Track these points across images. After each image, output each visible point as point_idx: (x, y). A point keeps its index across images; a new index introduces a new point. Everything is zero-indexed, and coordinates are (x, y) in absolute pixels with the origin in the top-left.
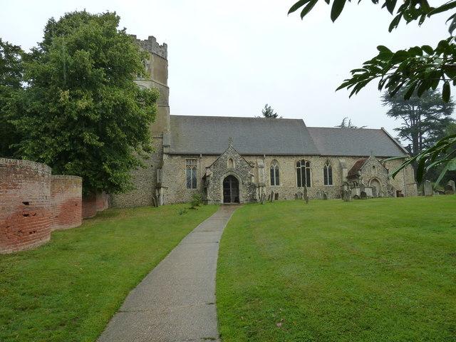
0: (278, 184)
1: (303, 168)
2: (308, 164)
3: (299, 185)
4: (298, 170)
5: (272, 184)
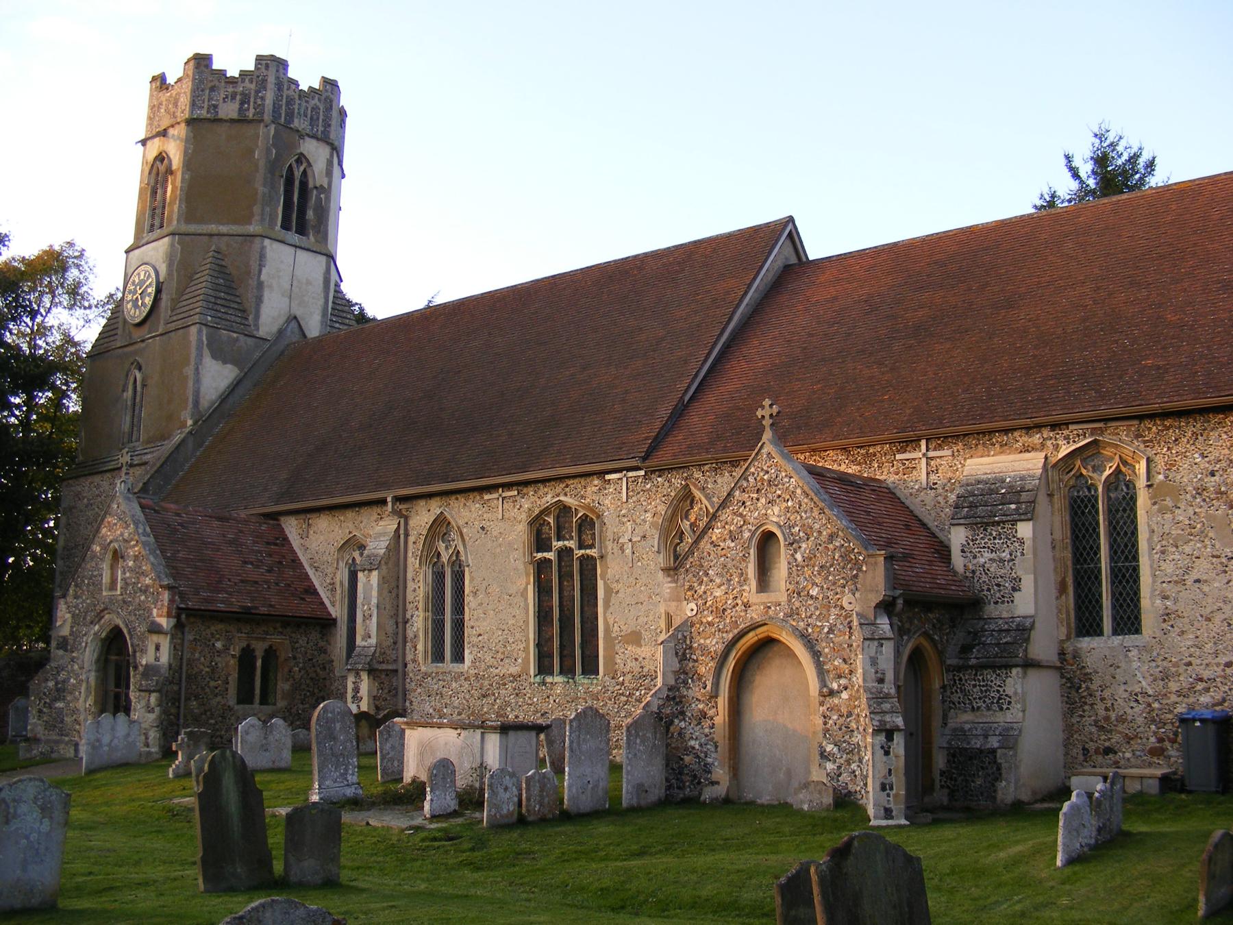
0: (459, 657)
1: (564, 553)
2: (586, 524)
3: (544, 668)
4: (541, 568)
5: (438, 656)
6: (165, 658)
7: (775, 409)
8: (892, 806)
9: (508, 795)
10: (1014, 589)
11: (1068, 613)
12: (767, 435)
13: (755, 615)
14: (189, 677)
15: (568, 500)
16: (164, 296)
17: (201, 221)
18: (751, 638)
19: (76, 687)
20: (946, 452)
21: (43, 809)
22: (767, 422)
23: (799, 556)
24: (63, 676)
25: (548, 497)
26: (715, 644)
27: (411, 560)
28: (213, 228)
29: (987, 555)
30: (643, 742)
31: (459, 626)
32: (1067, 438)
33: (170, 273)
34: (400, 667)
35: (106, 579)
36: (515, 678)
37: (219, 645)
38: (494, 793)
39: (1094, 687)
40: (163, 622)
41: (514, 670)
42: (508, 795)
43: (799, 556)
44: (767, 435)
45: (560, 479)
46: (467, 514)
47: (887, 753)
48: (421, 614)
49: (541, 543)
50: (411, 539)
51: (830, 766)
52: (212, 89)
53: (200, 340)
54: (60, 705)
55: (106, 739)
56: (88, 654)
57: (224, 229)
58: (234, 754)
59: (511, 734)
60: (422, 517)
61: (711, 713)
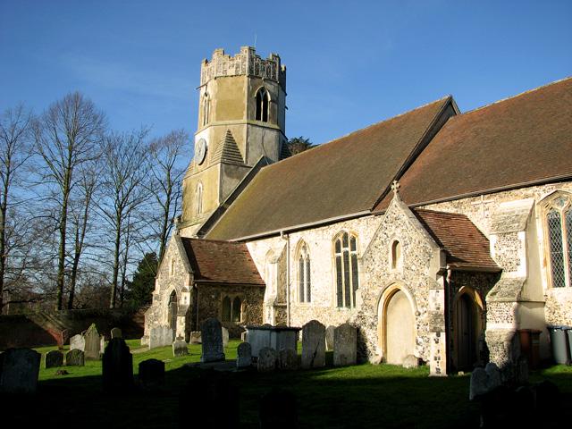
0: (309, 300)
1: (346, 254)
3: (340, 304)
4: (338, 260)
5: (302, 300)
6: (188, 303)
7: (398, 185)
8: (439, 367)
9: (269, 359)
10: (517, 264)
11: (548, 276)
12: (396, 196)
13: (391, 278)
14: (200, 310)
15: (347, 230)
16: (208, 152)
17: (222, 120)
18: (390, 290)
19: (161, 316)
20: (492, 200)
21: (29, 360)
22: (395, 191)
23: (407, 251)
24: (157, 310)
25: (338, 228)
26: (377, 292)
27: (291, 259)
28: (227, 122)
29: (506, 248)
30: (344, 336)
31: (309, 286)
32: (544, 190)
33: (210, 142)
34: (287, 304)
35: (170, 271)
36: (329, 309)
37: (213, 296)
38: (262, 357)
39: (561, 312)
40: (187, 287)
41: (329, 305)
42: (269, 359)
43: (407, 251)
44: (396, 196)
45: (357, 217)
46: (310, 236)
47: (437, 342)
48: (295, 281)
49: (338, 250)
50: (291, 250)
51: (420, 348)
52: (224, 64)
53: (221, 170)
54: (156, 322)
55: (158, 336)
56: (166, 300)
57: (231, 122)
58: (108, 338)
59: (282, 333)
60: (295, 237)
61: (375, 323)
